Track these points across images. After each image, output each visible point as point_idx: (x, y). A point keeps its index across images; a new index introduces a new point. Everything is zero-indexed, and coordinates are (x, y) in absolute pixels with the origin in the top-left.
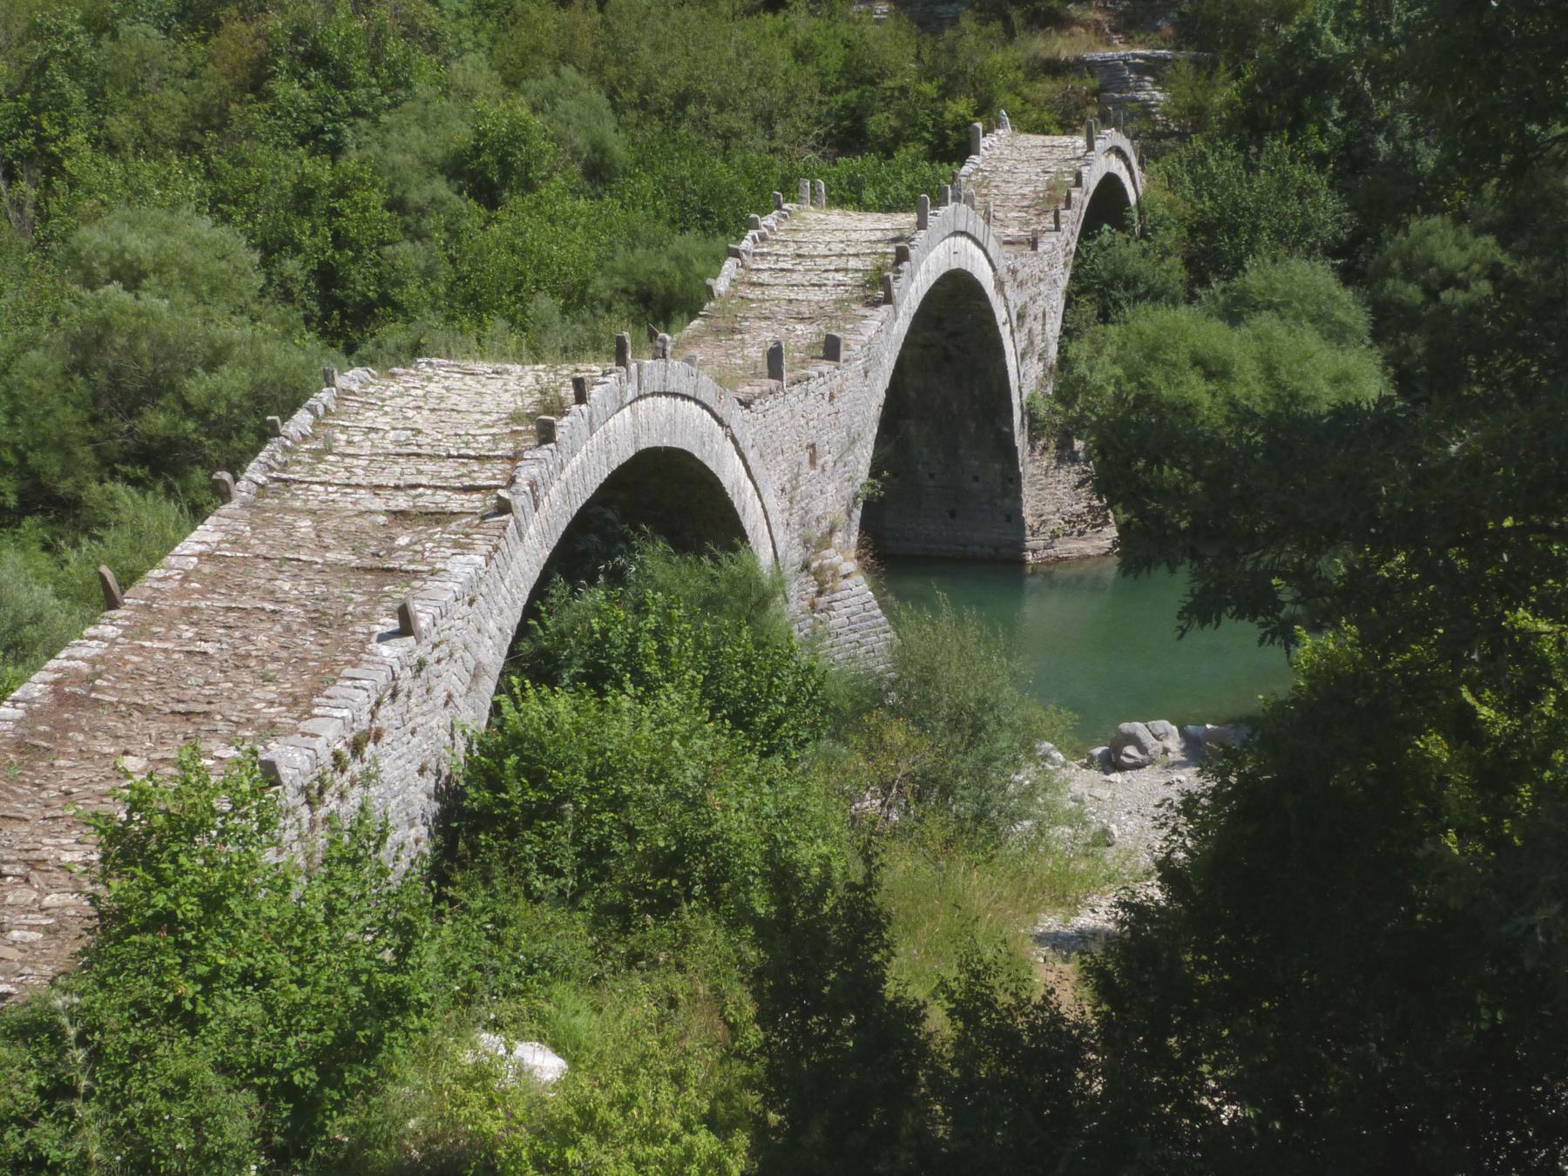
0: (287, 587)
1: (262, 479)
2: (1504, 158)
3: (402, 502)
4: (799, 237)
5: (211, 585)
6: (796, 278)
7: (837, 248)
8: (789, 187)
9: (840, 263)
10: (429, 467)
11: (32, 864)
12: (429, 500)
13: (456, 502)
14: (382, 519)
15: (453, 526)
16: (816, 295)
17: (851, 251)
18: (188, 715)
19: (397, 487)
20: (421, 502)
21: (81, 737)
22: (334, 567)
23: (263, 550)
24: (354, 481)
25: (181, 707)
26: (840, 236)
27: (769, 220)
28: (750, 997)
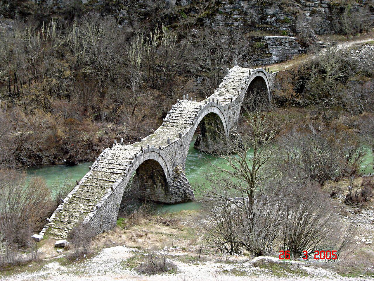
0: (98, 183)
1: (95, 167)
2: (205, 222)
3: (112, 171)
4: (180, 109)
5: (89, 181)
6: (179, 118)
7: (186, 112)
8: (181, 97)
9: (186, 115)
10: (116, 166)
11: (72, 216)
12: (116, 171)
13: (119, 172)
14: (110, 173)
15: (118, 175)
16: (181, 122)
17: (189, 113)
18: (87, 200)
19: (111, 169)
20: (114, 171)
21: (76, 202)
22: (104, 180)
23: (95, 177)
24: (106, 167)
25: (87, 198)
26: (187, 109)
27: (176, 105)
28: (154, 216)
